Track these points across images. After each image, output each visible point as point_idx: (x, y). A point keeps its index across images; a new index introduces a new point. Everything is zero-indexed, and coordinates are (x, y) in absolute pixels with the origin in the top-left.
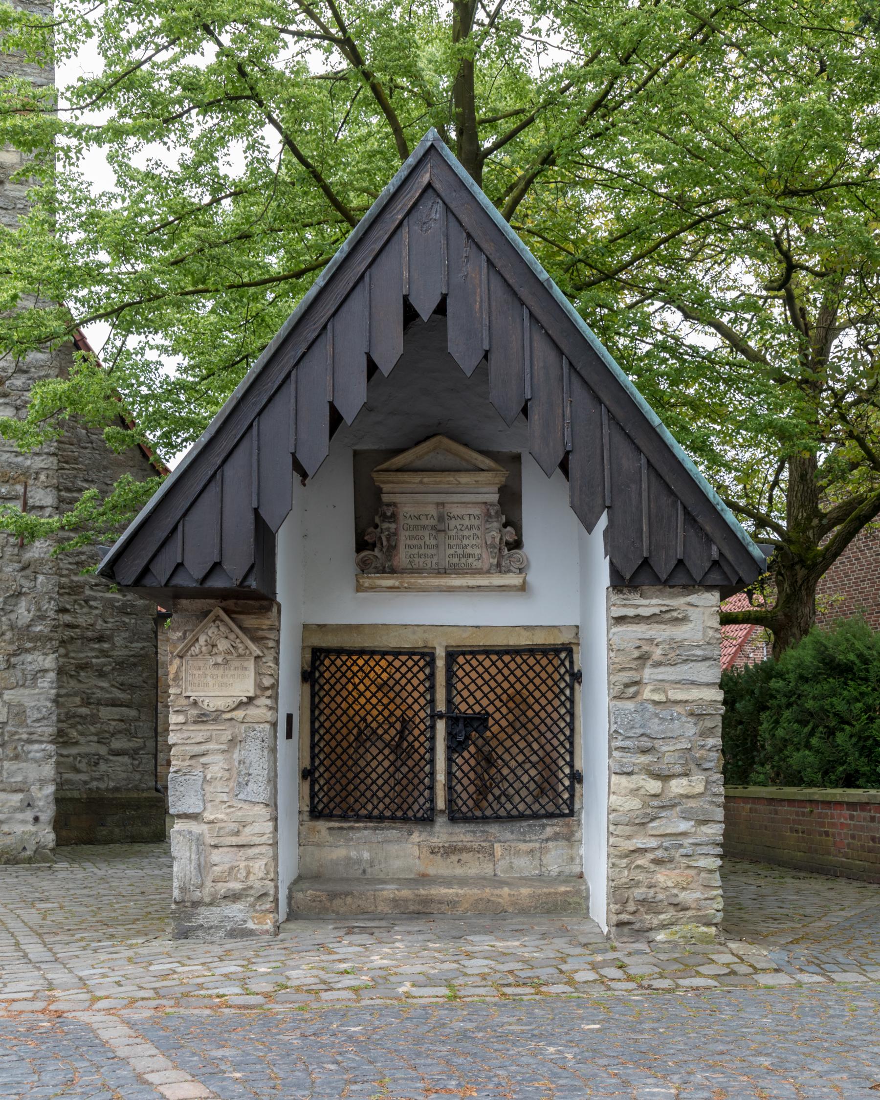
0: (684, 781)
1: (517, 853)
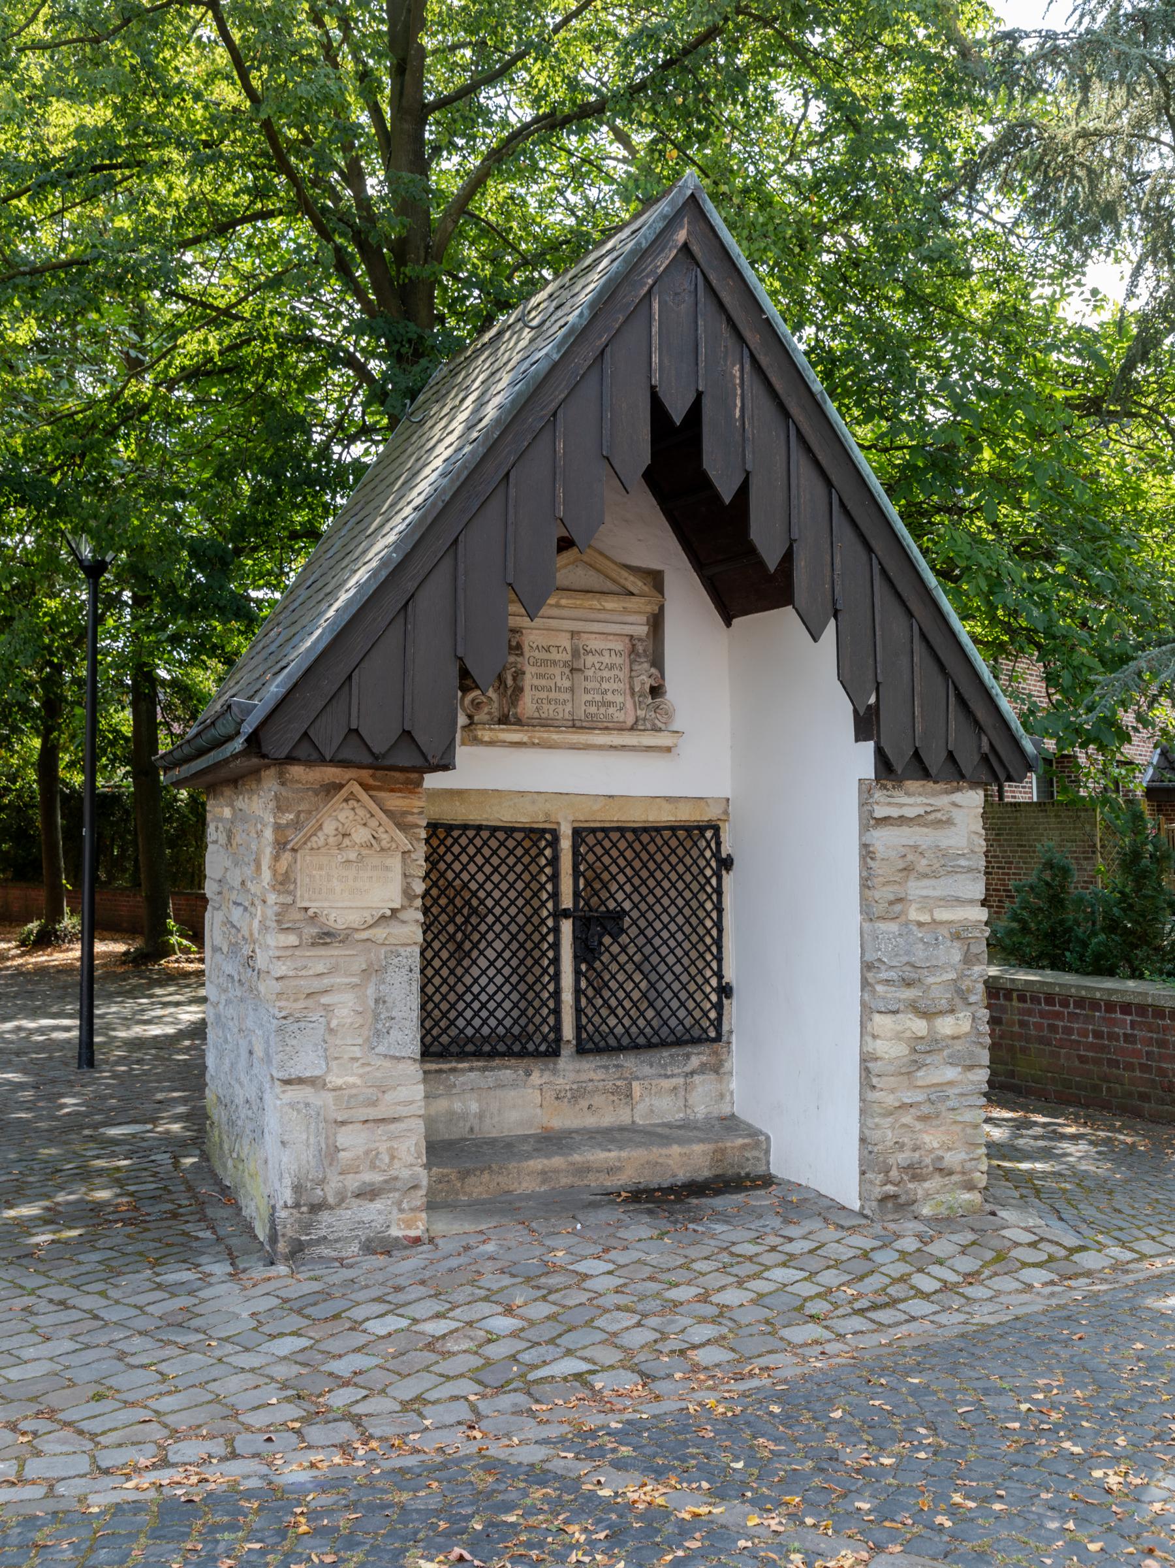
1: (659, 1093)
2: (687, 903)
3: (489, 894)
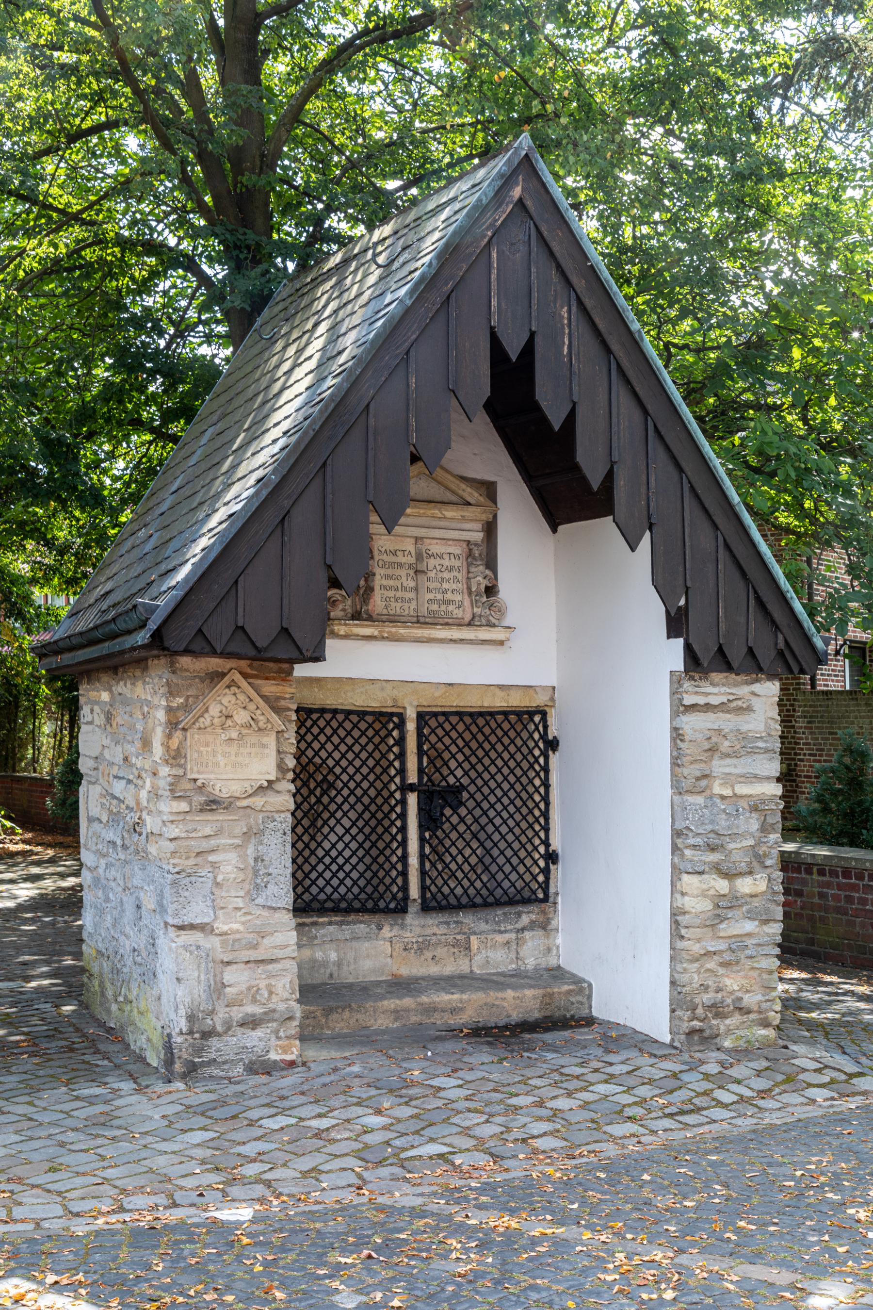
0: (748, 880)
1: (494, 946)
2: (518, 779)
3: (344, 770)
